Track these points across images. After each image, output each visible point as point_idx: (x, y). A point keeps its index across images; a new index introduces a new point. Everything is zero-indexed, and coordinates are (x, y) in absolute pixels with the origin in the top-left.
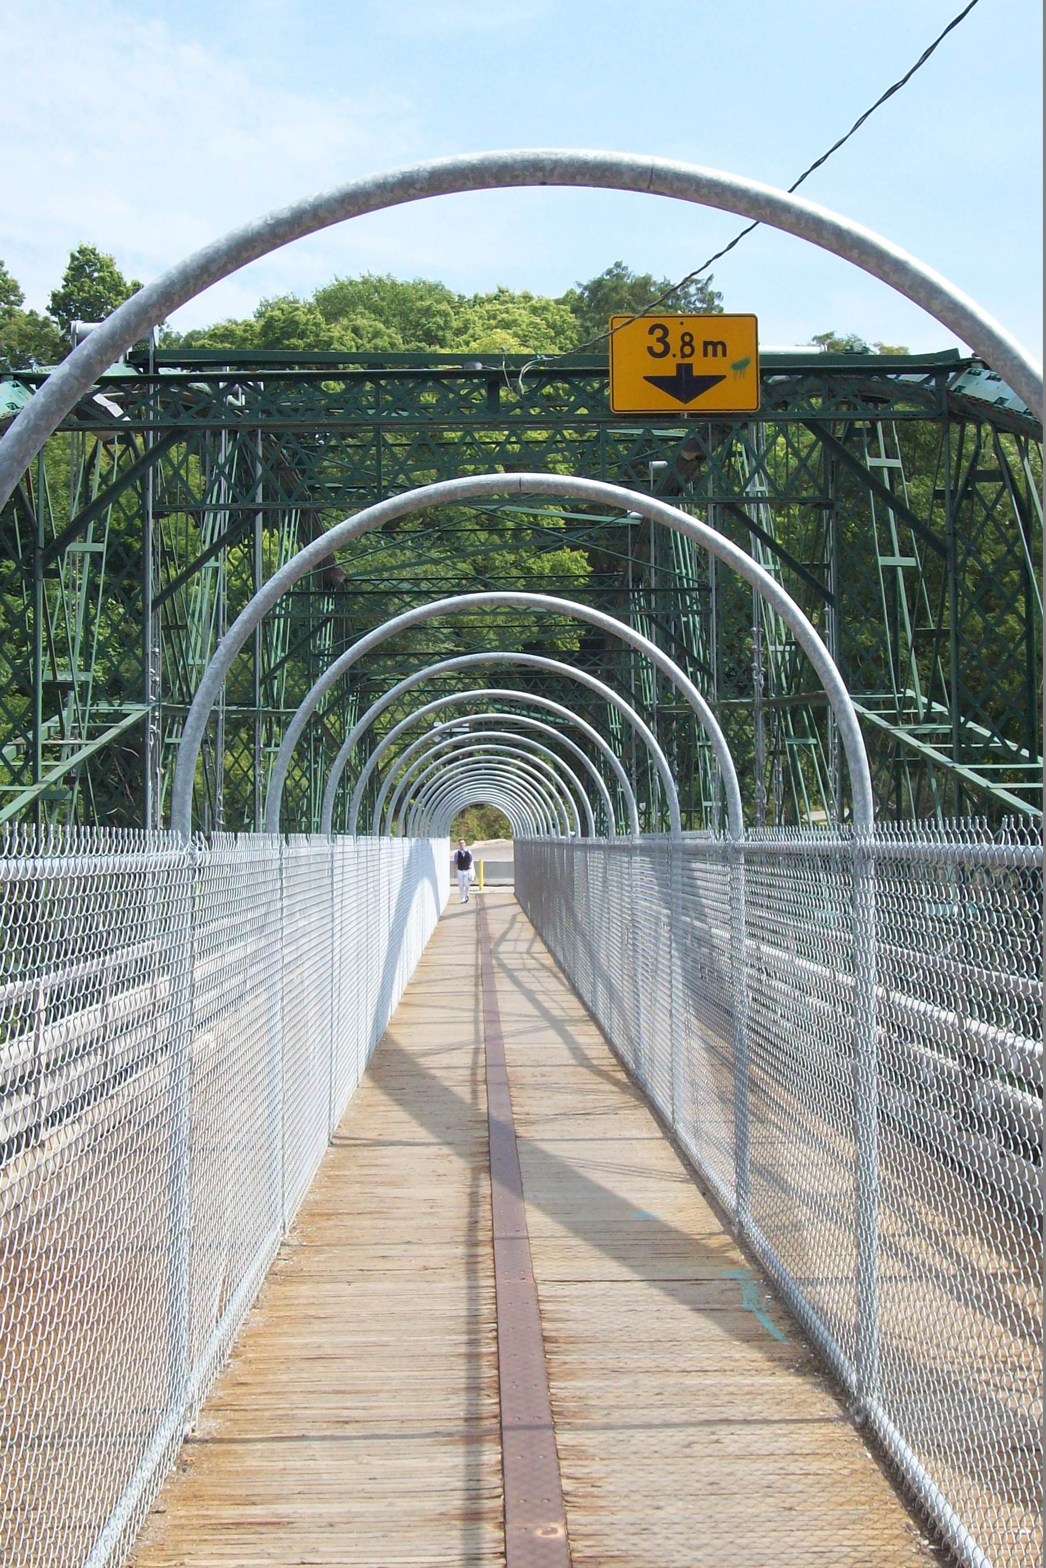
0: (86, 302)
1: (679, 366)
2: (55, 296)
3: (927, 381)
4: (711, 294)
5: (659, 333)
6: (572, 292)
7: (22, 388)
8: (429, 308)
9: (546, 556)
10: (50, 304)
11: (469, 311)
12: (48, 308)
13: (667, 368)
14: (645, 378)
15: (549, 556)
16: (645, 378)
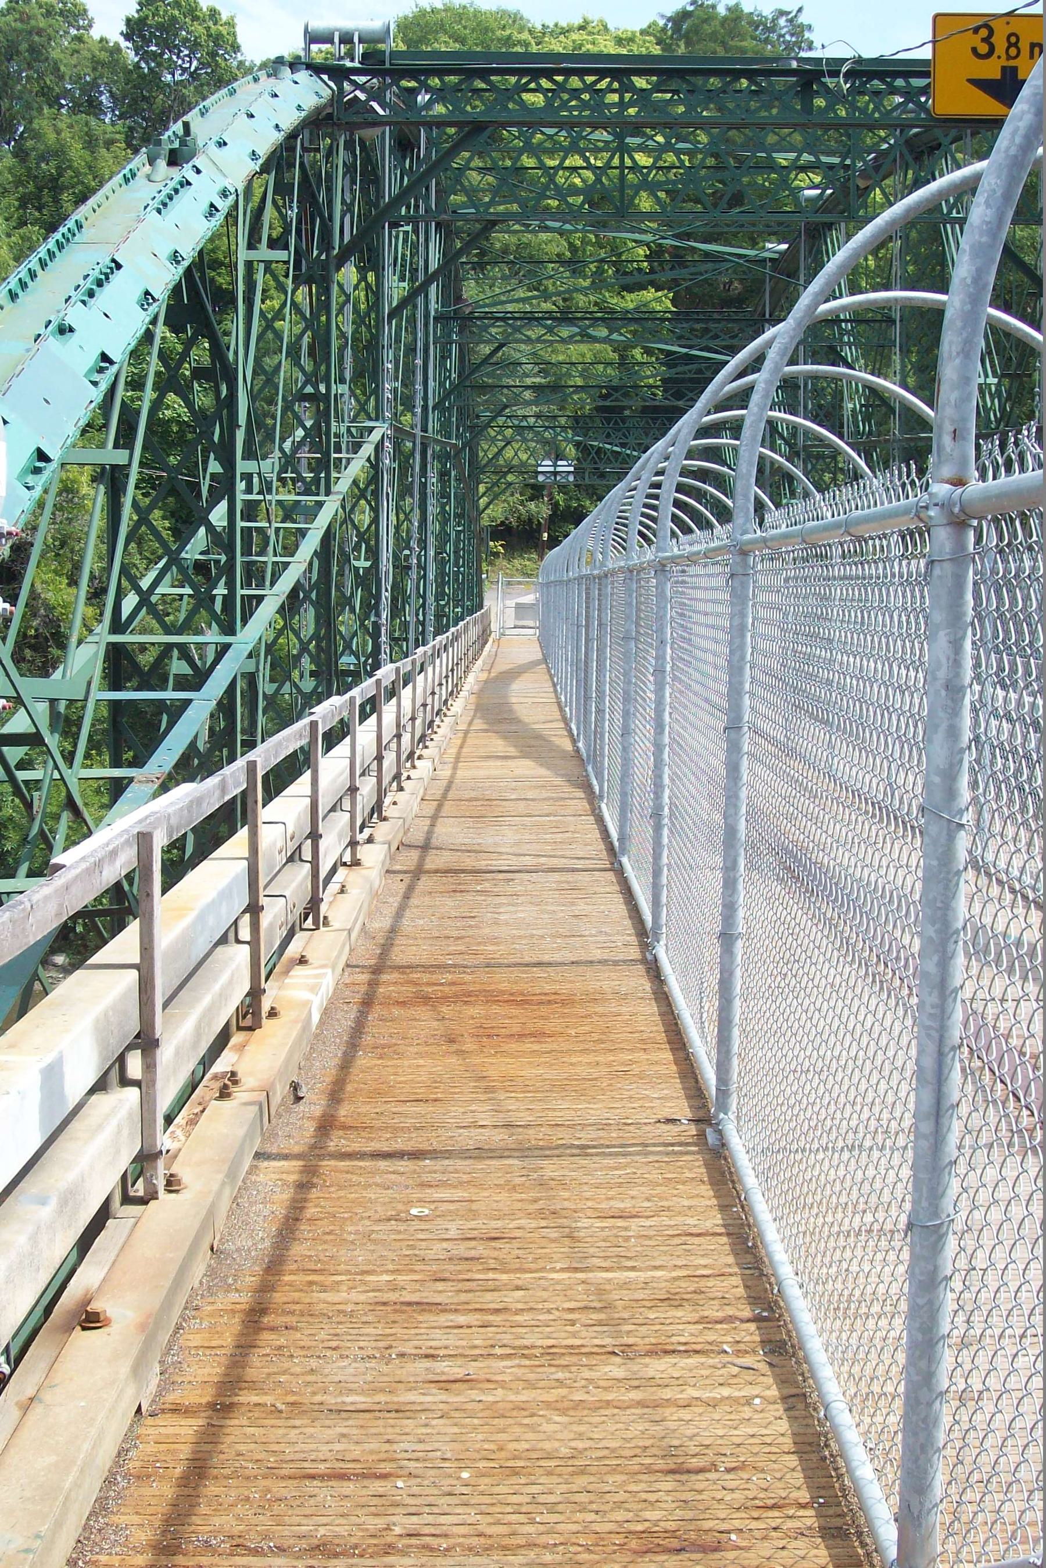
0: (161, 27)
1: (1004, 68)
2: (128, 21)
3: (519, 80)
4: (801, 26)
5: (984, 33)
6: (655, 23)
7: (315, 78)
8: (509, 37)
9: (629, 297)
10: (124, 29)
11: (553, 41)
12: (122, 33)
13: (991, 70)
14: (969, 80)
15: (633, 296)
16: (969, 80)
